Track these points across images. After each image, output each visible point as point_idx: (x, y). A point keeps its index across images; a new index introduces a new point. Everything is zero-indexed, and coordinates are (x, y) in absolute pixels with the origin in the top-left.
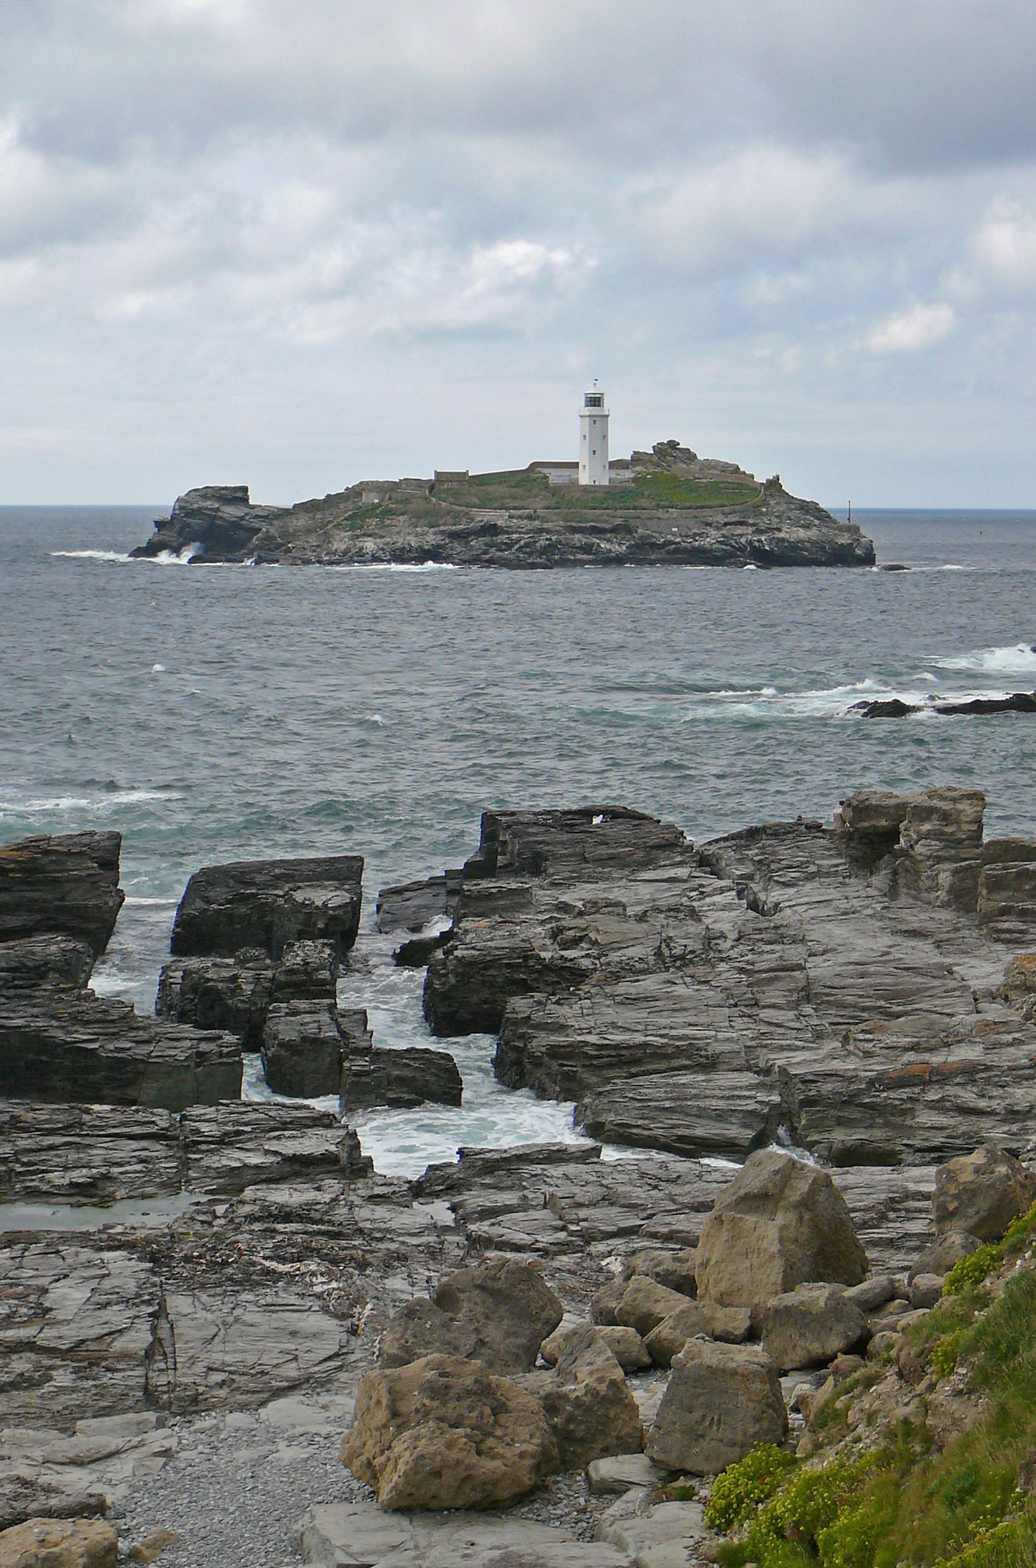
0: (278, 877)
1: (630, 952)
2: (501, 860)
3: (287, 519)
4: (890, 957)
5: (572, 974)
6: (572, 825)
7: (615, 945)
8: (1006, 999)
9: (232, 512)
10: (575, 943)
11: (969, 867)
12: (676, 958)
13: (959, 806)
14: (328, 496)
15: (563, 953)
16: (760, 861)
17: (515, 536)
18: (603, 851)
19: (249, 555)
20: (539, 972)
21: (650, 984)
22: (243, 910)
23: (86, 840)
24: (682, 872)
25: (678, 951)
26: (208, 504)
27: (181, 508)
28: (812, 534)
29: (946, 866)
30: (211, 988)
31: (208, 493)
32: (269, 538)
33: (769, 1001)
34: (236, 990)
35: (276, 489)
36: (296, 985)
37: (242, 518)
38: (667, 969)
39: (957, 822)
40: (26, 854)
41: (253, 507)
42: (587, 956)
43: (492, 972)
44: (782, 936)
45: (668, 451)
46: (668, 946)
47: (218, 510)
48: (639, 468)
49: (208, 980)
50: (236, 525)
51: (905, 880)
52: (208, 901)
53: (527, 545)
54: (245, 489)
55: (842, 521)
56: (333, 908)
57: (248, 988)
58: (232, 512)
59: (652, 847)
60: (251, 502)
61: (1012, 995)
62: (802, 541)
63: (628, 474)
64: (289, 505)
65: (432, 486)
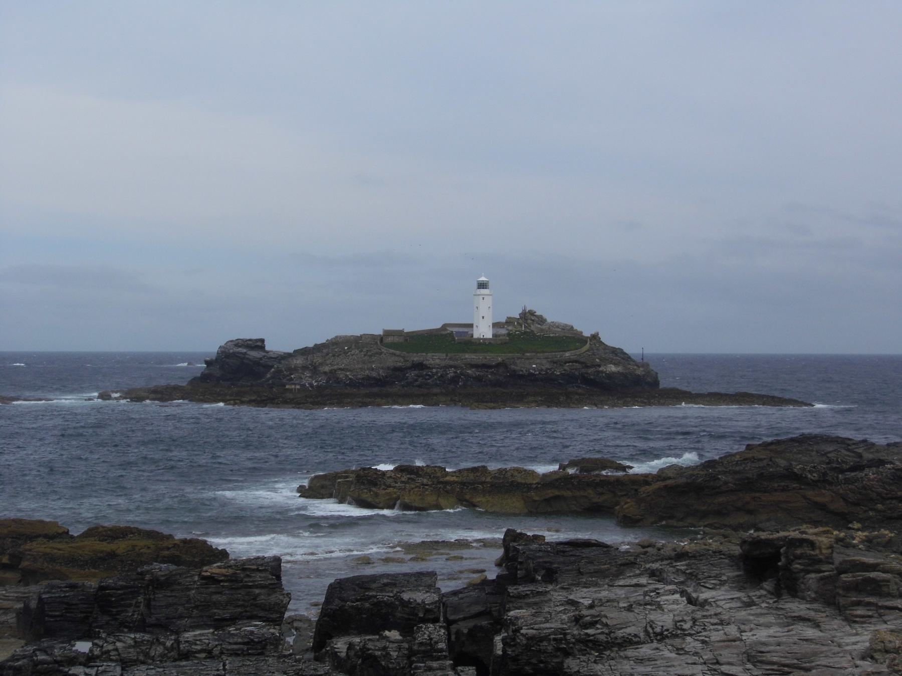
0: (386, 585)
1: (628, 630)
2: (520, 573)
3: (290, 360)
4: (794, 632)
5: (594, 644)
6: (564, 552)
7: (619, 626)
8: (872, 658)
9: (255, 354)
10: (592, 624)
11: (830, 576)
12: (656, 634)
13: (820, 539)
14: (316, 345)
15: (586, 631)
16: (690, 574)
17: (434, 370)
18: (592, 568)
19: (96, 389)
20: (574, 643)
21: (645, 650)
22: (367, 605)
23: (260, 562)
24: (643, 580)
25: (658, 630)
26: (240, 349)
27: (222, 352)
28: (620, 369)
29: (813, 575)
30: (370, 654)
31: (240, 343)
32: (279, 371)
33: (725, 660)
34: (387, 655)
35: (281, 341)
36: (424, 652)
37: (261, 359)
38: (652, 642)
39: (820, 548)
40: (231, 571)
41: (267, 352)
42: (602, 633)
43: (545, 643)
44: (722, 621)
45: (528, 316)
46: (651, 626)
47: (245, 354)
48: (510, 328)
49: (369, 649)
50: (257, 362)
51: (789, 587)
52: (343, 600)
53: (441, 376)
54: (262, 341)
55: (638, 360)
56: (429, 604)
57: (394, 654)
58: (255, 354)
59: (621, 565)
60: (267, 348)
61: (876, 656)
62: (614, 373)
63: (503, 331)
64: (291, 351)
65: (382, 338)
